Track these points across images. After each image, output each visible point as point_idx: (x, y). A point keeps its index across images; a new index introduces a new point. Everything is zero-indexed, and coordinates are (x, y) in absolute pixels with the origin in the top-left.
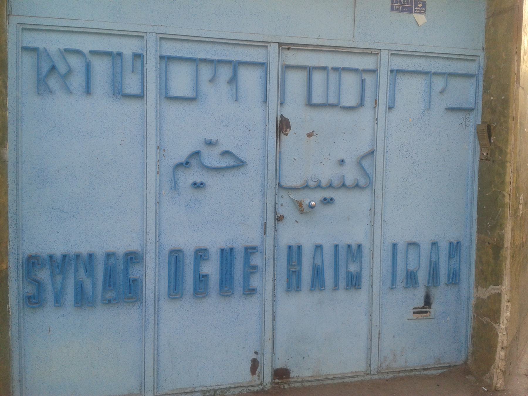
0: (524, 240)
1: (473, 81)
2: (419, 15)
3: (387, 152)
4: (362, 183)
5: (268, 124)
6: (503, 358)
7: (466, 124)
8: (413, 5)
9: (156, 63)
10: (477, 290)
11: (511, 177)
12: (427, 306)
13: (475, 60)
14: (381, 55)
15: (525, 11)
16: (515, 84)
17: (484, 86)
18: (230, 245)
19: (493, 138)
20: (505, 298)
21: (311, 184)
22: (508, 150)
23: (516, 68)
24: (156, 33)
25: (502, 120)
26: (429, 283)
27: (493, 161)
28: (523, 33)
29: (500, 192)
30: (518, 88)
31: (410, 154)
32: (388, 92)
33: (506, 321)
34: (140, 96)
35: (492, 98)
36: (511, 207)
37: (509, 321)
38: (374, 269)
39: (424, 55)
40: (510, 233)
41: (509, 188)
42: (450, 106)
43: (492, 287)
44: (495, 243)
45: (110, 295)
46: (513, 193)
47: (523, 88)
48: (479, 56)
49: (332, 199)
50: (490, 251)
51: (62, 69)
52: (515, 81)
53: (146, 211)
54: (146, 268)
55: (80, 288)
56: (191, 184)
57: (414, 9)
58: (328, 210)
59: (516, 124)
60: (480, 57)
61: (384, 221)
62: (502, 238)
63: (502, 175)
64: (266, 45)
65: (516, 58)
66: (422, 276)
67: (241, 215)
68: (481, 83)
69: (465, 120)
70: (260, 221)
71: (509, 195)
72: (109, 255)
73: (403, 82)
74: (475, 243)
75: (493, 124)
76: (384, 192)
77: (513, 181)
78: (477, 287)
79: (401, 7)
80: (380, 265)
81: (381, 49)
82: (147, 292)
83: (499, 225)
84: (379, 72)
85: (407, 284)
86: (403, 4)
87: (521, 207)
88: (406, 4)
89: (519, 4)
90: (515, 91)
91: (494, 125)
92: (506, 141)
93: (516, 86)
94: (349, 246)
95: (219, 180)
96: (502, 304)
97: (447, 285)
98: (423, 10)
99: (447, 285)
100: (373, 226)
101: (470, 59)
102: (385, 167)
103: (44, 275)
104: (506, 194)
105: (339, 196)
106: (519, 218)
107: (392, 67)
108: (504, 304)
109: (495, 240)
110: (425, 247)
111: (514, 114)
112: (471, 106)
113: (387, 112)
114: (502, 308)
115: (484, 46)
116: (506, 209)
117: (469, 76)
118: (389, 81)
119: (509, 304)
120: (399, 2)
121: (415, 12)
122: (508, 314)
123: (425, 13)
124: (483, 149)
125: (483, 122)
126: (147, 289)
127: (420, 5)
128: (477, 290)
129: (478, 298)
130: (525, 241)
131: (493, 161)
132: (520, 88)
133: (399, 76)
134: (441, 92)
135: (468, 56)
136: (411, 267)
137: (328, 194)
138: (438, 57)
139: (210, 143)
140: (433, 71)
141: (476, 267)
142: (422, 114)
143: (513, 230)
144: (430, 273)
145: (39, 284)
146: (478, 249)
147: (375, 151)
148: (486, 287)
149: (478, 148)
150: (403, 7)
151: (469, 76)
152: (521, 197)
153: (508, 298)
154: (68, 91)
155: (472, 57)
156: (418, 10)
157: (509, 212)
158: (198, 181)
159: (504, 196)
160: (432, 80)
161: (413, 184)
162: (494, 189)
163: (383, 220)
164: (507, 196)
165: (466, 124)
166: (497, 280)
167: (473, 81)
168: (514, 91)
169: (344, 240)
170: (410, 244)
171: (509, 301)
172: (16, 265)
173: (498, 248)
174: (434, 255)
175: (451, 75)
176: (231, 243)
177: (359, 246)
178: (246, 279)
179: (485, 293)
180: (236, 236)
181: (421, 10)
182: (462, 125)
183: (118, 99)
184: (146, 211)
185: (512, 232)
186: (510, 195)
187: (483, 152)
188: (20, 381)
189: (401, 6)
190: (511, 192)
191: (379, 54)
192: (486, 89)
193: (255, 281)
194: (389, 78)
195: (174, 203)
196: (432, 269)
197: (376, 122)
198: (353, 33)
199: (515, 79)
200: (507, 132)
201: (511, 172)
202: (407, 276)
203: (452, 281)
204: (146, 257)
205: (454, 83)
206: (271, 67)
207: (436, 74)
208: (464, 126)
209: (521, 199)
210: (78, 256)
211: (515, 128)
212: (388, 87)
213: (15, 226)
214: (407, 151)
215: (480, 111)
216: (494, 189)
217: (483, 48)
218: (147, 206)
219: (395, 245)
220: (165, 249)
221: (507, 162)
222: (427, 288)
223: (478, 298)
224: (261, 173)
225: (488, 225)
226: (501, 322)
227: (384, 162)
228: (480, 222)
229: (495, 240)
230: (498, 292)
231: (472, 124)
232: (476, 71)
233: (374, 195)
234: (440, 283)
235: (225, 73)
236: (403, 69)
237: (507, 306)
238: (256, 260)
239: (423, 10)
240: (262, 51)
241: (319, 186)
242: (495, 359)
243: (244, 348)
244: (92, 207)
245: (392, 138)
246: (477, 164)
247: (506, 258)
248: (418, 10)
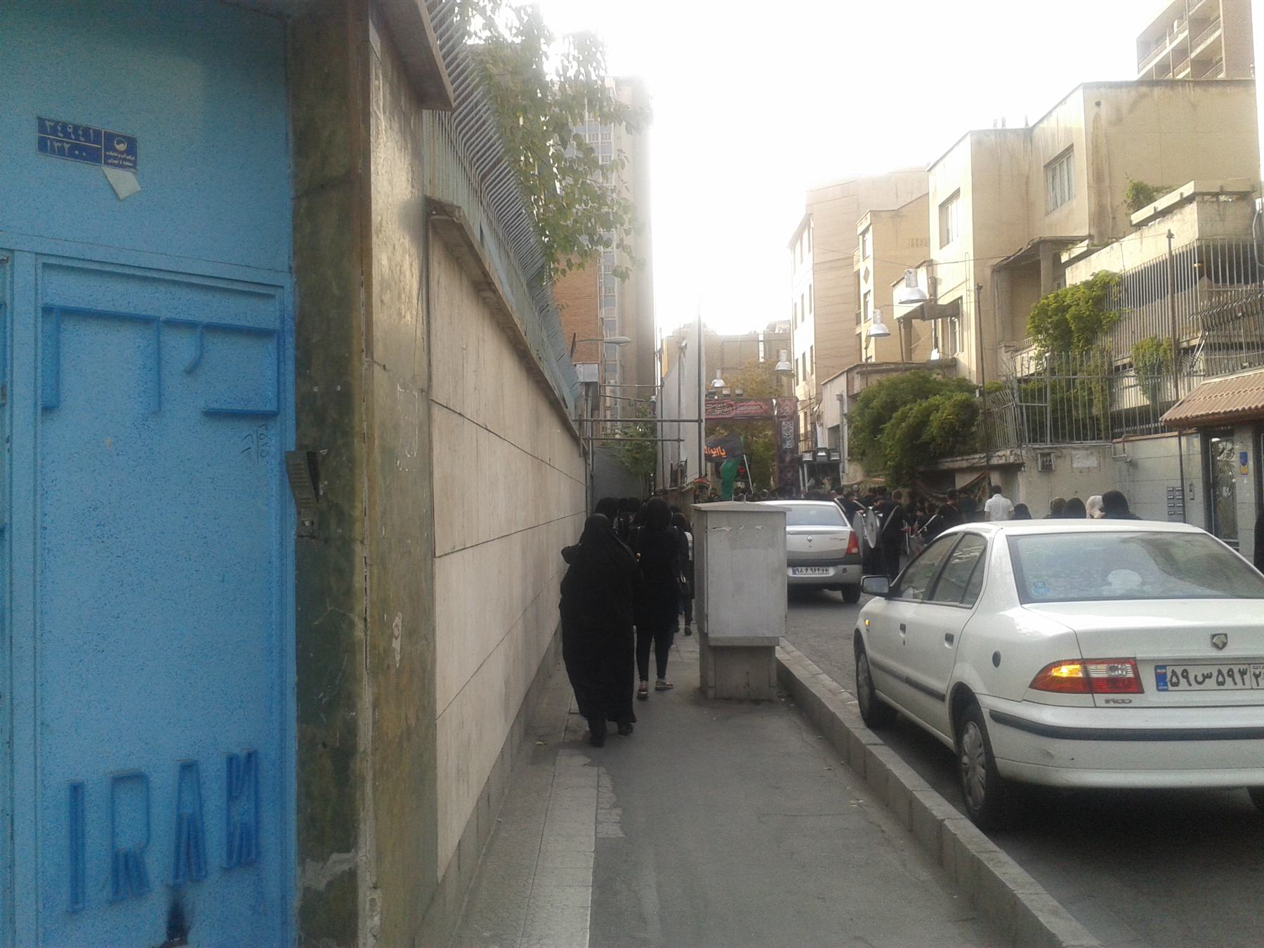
0: (413, 722)
1: (270, 346)
2: (119, 172)
3: (45, 528)
7: (260, 451)
8: (101, 144)
10: (304, 871)
11: (366, 576)
12: (175, 939)
13: (272, 296)
14: (12, 266)
15: (376, 188)
16: (364, 357)
17: (297, 360)
19: (323, 484)
20: (366, 879)
22: (357, 513)
23: (363, 318)
25: (340, 442)
26: (176, 876)
27: (326, 541)
28: (374, 238)
29: (344, 614)
30: (371, 366)
32: (39, 365)
33: (373, 938)
35: (316, 389)
36: (370, 650)
37: (378, 936)
38: (17, 869)
39: (138, 273)
40: (369, 713)
41: (362, 604)
42: (216, 406)
43: (334, 856)
44: (338, 745)
46: (372, 616)
47: (384, 366)
48: (282, 287)
52: (363, 351)
57: (105, 154)
59: (370, 452)
60: (285, 288)
61: (42, 724)
62: (351, 730)
63: (345, 573)
65: (363, 296)
66: (158, 864)
68: (290, 352)
69: (255, 442)
71: (363, 622)
74: (292, 747)
75: (321, 451)
76: (38, 641)
77: (371, 586)
78: (302, 862)
79: (67, 146)
81: (12, 251)
83: (344, 698)
84: (8, 312)
85: (116, 892)
86: (73, 137)
87: (396, 644)
88: (81, 139)
89: (360, 171)
90: (364, 374)
91: (324, 452)
92: (351, 493)
93: (366, 361)
96: (359, 897)
97: (227, 870)
98: (129, 160)
99: (227, 870)
100: (8, 743)
101: (259, 292)
102: (38, 571)
104: (356, 619)
106: (393, 671)
107: (47, 300)
108: (366, 895)
109: (338, 736)
110: (164, 780)
111: (365, 427)
112: (271, 407)
113: (39, 418)
114: (360, 907)
115: (293, 265)
116: (358, 657)
117: (260, 334)
118: (40, 336)
119: (377, 895)
120: (70, 133)
121: (106, 163)
122: (377, 919)
123: (134, 167)
124: (303, 510)
125: (300, 446)
127: (122, 147)
128: (304, 871)
129: (307, 889)
130: (414, 725)
131: (326, 541)
132: (375, 366)
133: (69, 325)
134: (191, 371)
136: (126, 842)
138: (175, 283)
140: (165, 315)
141: (299, 811)
143: (375, 706)
144: (178, 848)
146: (302, 764)
147: (8, 527)
149: (292, 510)
150: (74, 147)
151: (260, 334)
152: (398, 620)
153: (374, 879)
155: (242, 284)
156: (115, 158)
157: (363, 661)
159: (352, 624)
160: (162, 339)
162: (329, 609)
163: (39, 723)
164: (360, 625)
165: (260, 451)
166: (345, 837)
167: (271, 346)
168: (361, 375)
170: (119, 780)
171: (375, 887)
173: (344, 754)
175: (212, 328)
179: (320, 876)
181: (125, 159)
182: (249, 453)
185: (374, 711)
186: (365, 620)
187: (303, 519)
189: (67, 143)
190: (368, 613)
191: (9, 263)
192: (303, 364)
194: (39, 329)
196: (184, 837)
197: (8, 445)
199: (363, 346)
200: (352, 470)
201: (366, 563)
202: (115, 871)
203: (240, 856)
205: (222, 350)
207: (172, 324)
209: (396, 625)
211: (368, 460)
212: (40, 351)
214: (103, 523)
215: (291, 423)
216: (329, 609)
217: (291, 268)
219: (76, 790)
222: (176, 892)
223: (307, 889)
227: (35, 557)
228: (304, 692)
229: (338, 736)
230: (350, 869)
231: (273, 449)
232: (278, 322)
233: (8, 653)
234: (206, 872)
236: (81, 306)
237: (373, 900)
239: (129, 160)
246: (291, 548)
247: (363, 779)
248: (115, 158)
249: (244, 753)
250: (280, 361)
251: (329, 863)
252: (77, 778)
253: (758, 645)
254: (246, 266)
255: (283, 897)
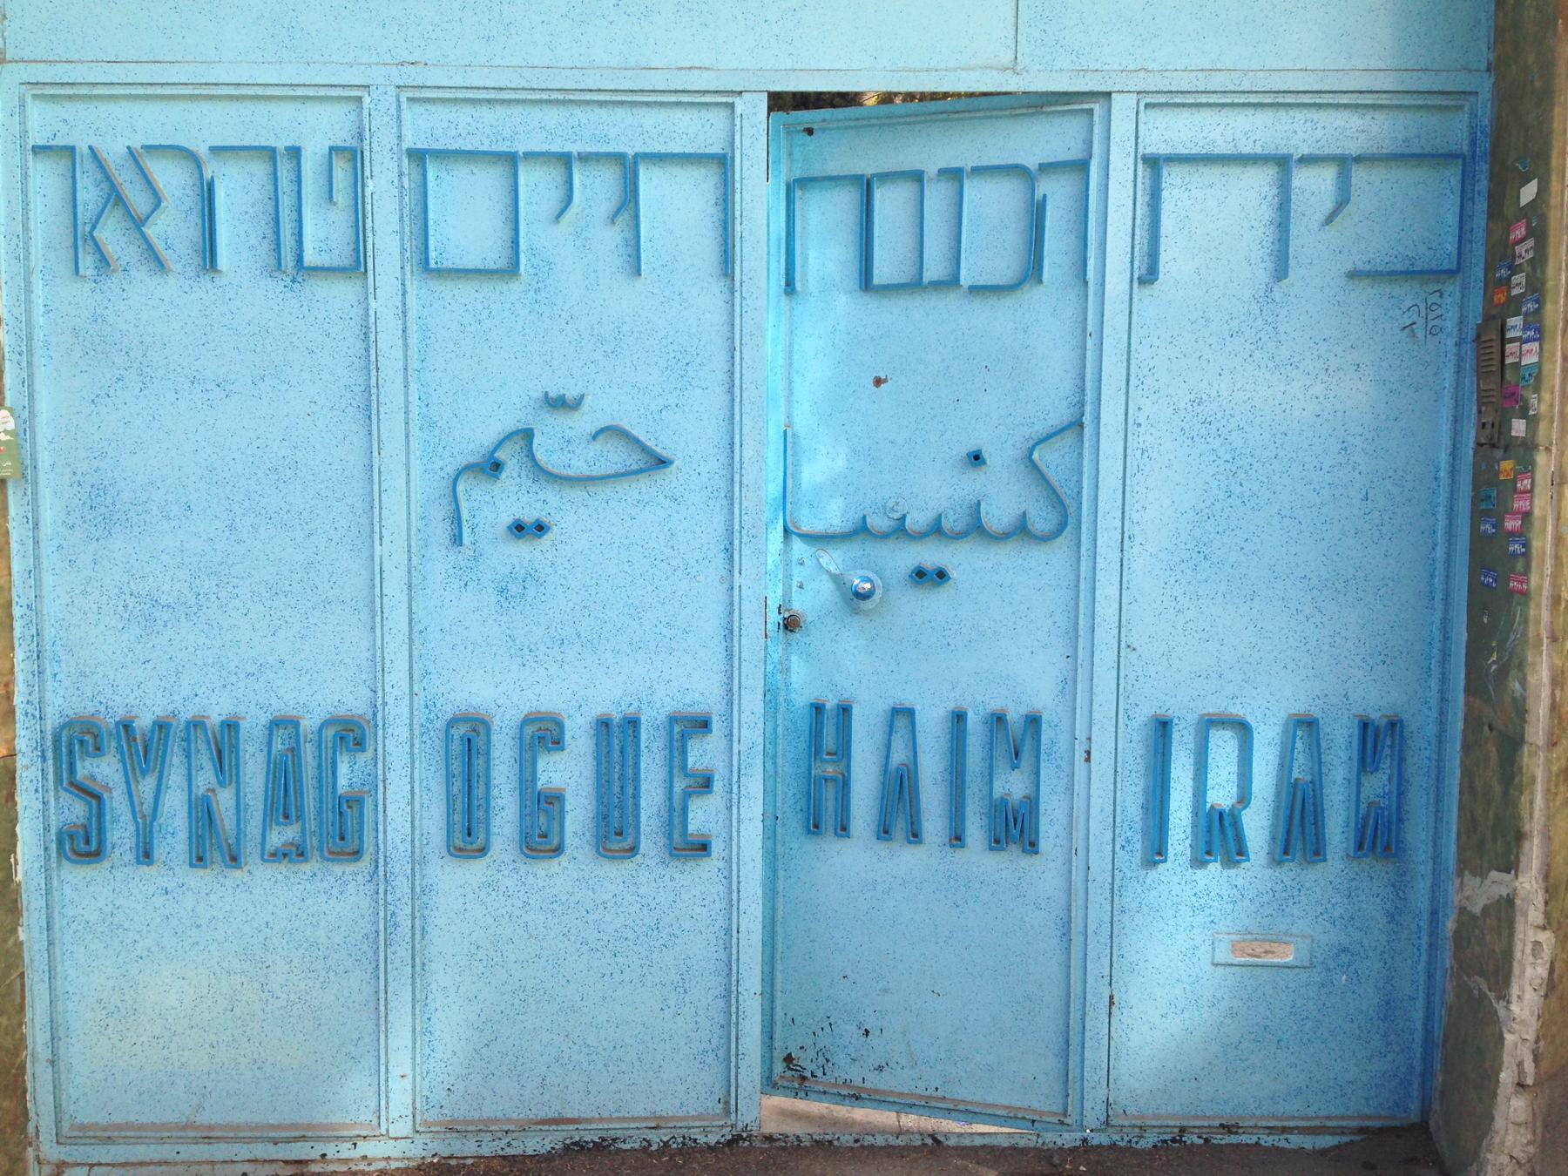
4: (1041, 520)
5: (741, 344)
6: (1522, 1118)
9: (401, 175)
18: (632, 710)
21: (878, 522)
24: (398, 87)
31: (1220, 432)
34: (356, 266)
43: (1494, 874)
45: (280, 836)
48: (1477, 93)
49: (942, 575)
50: (1492, 750)
51: (138, 200)
53: (382, 603)
54: (384, 768)
55: (203, 815)
56: (509, 528)
58: (935, 602)
64: (730, 100)
66: (1257, 825)
67: (663, 623)
68: (1483, 185)
69: (1423, 314)
70: (723, 642)
72: (283, 724)
73: (444, 184)
78: (1460, 874)
80: (1115, 787)
82: (389, 838)
94: (998, 720)
95: (595, 516)
103: (105, 769)
105: (955, 557)
112: (1446, 266)
124: (1484, 408)
126: (389, 828)
135: (1304, 96)
136: (1221, 794)
137: (930, 555)
139: (559, 404)
142: (1261, 300)
145: (91, 794)
148: (1481, 873)
154: (155, 260)
158: (529, 517)
161: (1233, 530)
165: (1430, 326)
169: (980, 701)
172: (36, 748)
174: (1300, 759)
176: (635, 705)
177: (1034, 721)
178: (676, 813)
180: (648, 685)
182: (1413, 331)
183: (296, 285)
184: (382, 603)
188: (52, 1063)
193: (703, 816)
195: (463, 583)
198: (1013, 46)
204: (384, 738)
206: (745, 168)
208: (1420, 335)
210: (197, 724)
213: (32, 641)
214: (1208, 420)
218: (385, 592)
219: (1163, 726)
220: (440, 715)
221: (1536, 447)
224: (723, 495)
225: (1490, 666)
226: (1514, 998)
230: (1508, 895)
235: (594, 187)
238: (703, 753)
240: (718, 117)
241: (900, 531)
242: (1492, 1118)
243: (802, 1048)
244: (236, 591)
245: (1157, 380)
249: (1385, 721)
250: (1465, 198)
251: (1487, 882)
252: (1167, 714)
253: (216, 190)
254: (1421, 70)
255: (1434, 913)
